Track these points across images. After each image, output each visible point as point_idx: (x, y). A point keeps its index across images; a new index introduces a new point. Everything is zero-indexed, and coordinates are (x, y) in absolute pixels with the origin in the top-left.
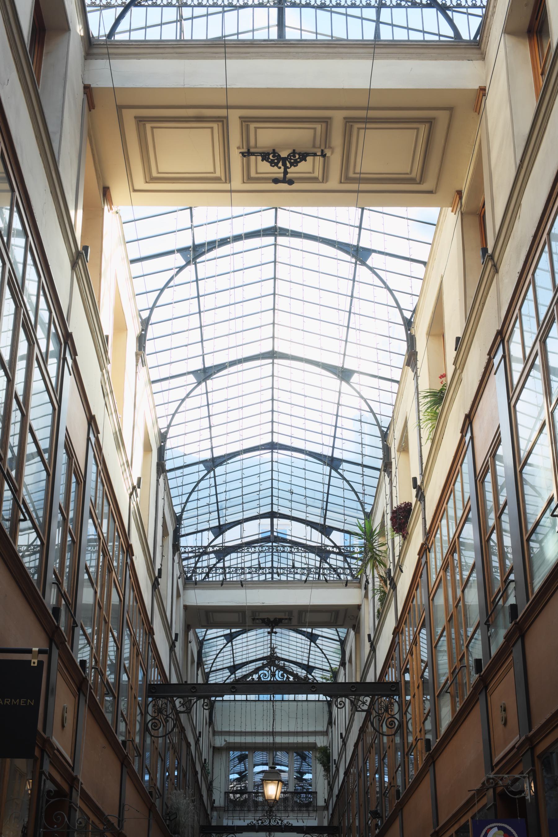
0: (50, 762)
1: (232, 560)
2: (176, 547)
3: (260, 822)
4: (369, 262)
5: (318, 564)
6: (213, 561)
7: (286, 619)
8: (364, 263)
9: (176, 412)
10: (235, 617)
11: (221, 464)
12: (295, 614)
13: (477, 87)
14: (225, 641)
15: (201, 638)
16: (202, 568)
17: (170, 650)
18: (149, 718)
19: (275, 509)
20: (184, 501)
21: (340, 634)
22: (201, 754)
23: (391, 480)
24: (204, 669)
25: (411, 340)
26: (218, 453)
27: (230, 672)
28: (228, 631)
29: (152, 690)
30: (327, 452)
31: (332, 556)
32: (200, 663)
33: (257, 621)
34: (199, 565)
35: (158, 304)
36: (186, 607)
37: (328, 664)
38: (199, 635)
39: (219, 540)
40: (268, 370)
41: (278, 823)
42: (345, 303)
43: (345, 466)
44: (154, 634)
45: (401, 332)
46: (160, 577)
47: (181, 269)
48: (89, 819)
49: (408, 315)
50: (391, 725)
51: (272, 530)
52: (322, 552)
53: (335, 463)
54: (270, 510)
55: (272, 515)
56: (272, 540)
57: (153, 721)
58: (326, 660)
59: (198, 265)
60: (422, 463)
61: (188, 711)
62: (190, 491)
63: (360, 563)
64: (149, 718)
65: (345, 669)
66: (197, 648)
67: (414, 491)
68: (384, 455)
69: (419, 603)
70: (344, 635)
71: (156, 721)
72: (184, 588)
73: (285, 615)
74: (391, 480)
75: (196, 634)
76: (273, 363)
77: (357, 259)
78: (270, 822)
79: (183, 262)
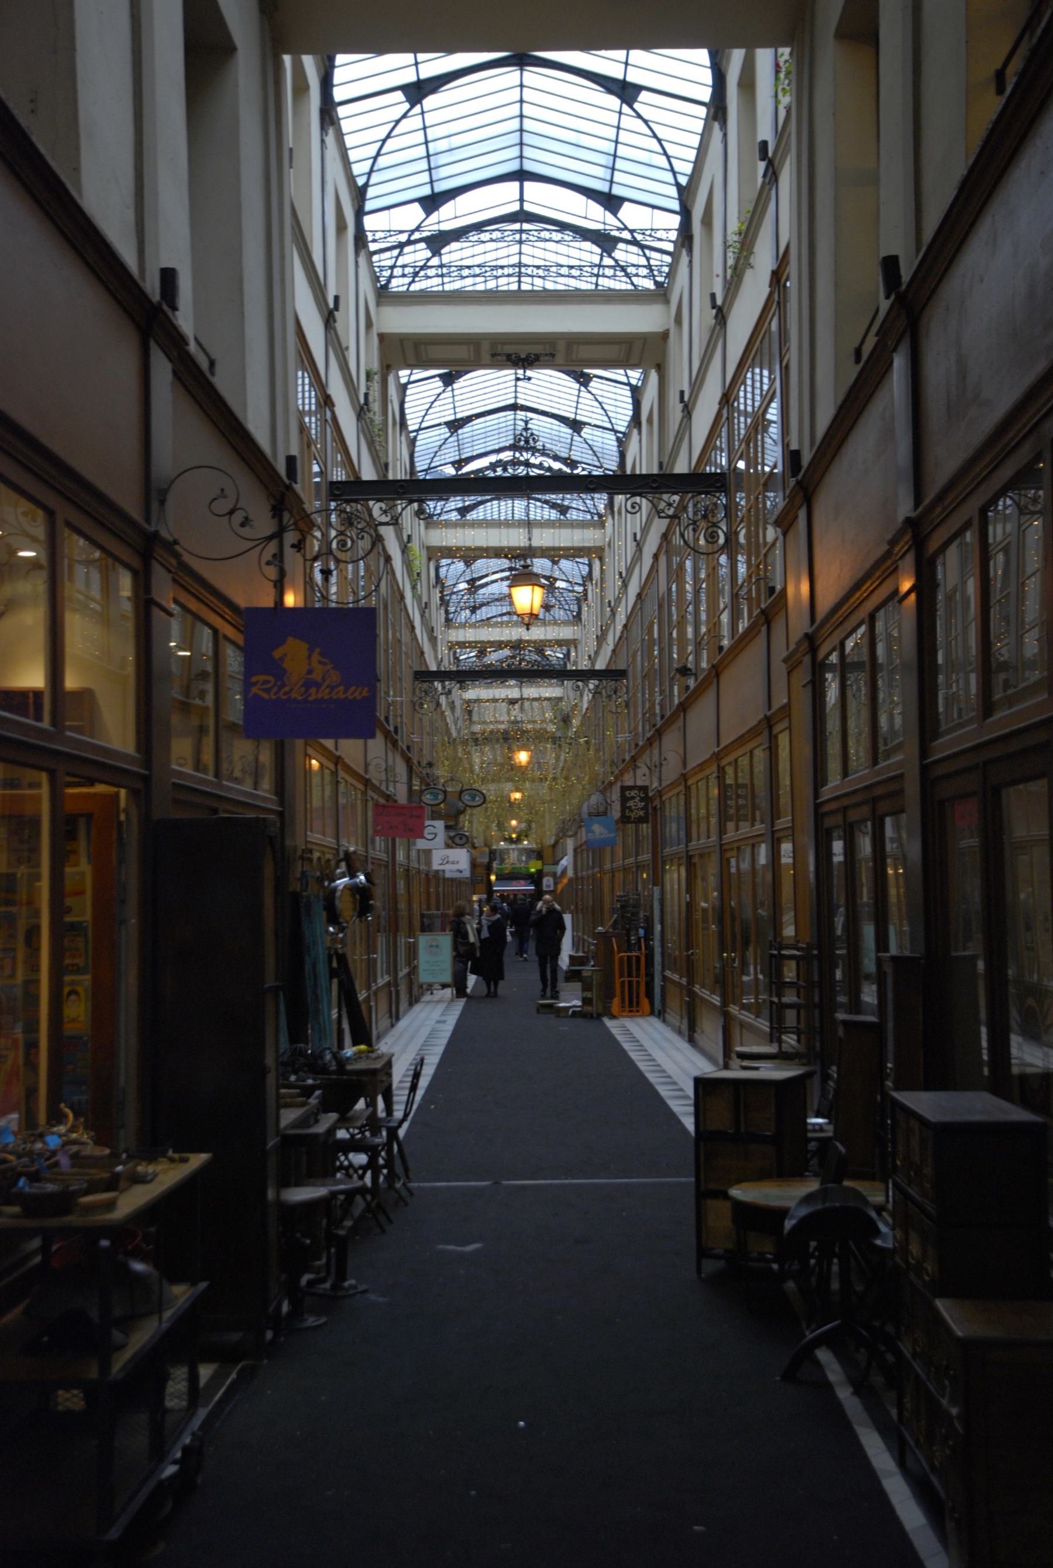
0: (174, 580)
1: (453, 253)
2: (361, 239)
5: (596, 260)
7: (546, 355)
11: (434, 91)
12: (561, 346)
13: (661, 330)
17: (358, 420)
18: (333, 533)
19: (520, 401)
23: (691, 262)
24: (398, 378)
26: (441, 187)
30: (603, 187)
31: (621, 246)
32: (403, 424)
33: (499, 358)
36: (382, 337)
42: (611, 133)
45: (673, 192)
47: (398, 122)
49: (683, 181)
50: (713, 537)
51: (522, 200)
52: (605, 241)
54: (518, 208)
55: (521, 176)
57: (339, 538)
58: (610, 414)
61: (395, 522)
62: (383, 137)
63: (668, 259)
64: (333, 533)
65: (640, 433)
66: (353, 205)
67: (762, 166)
72: (378, 304)
74: (691, 262)
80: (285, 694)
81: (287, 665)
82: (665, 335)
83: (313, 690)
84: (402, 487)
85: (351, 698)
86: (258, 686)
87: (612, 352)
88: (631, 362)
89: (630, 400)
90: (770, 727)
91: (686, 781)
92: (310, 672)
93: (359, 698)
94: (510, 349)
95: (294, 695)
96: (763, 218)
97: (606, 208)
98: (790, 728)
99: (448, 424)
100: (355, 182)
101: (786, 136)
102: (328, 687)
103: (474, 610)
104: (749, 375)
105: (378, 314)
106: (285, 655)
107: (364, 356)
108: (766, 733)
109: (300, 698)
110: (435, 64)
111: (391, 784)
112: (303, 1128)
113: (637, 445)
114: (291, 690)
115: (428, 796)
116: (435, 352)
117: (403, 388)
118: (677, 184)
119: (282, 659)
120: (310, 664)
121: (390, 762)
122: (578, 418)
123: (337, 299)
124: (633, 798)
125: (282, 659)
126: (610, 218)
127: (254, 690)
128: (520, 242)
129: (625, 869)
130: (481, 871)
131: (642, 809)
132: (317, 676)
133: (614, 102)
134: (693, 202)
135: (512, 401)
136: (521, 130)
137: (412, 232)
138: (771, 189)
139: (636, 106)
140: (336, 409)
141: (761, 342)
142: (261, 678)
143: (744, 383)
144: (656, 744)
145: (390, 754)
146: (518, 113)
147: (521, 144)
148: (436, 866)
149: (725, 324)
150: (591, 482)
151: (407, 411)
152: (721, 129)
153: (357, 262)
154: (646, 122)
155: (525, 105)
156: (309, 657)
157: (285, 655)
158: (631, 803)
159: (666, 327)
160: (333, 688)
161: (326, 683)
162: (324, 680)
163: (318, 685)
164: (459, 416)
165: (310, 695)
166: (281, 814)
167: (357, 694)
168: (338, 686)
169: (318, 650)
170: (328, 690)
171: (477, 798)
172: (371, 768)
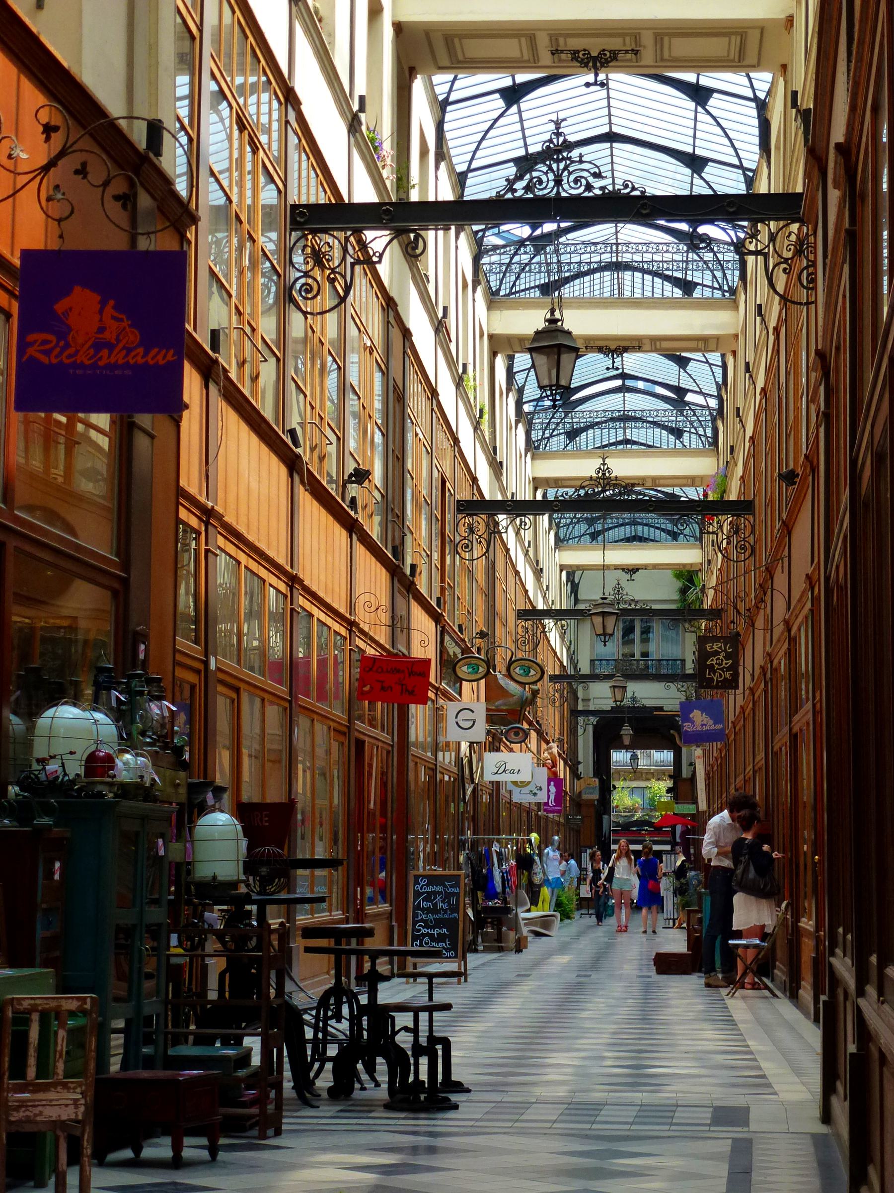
3: (520, 185)
7: (627, 52)
10: (511, 49)
13: (783, 16)
14: (501, 103)
15: (441, 98)
19: (615, 129)
21: (756, 84)
28: (507, 82)
29: (307, 219)
33: (563, 56)
38: (438, 90)
41: (589, 187)
44: (301, 104)
48: (239, 563)
60: (289, 841)
70: (766, 87)
71: (310, 281)
73: (624, 44)
75: (432, 86)
76: (611, 147)
78: (558, 182)
83: (105, 352)
85: (151, 363)
86: (36, 347)
87: (716, 47)
88: (746, 63)
89: (756, 122)
92: (101, 330)
93: (161, 362)
94: (575, 43)
99: (516, 161)
102: (124, 348)
106: (71, 309)
107: (372, 71)
109: (88, 362)
113: (767, 181)
114: (77, 352)
115: (465, 668)
117: (442, 106)
121: (401, 611)
122: (698, 152)
124: (716, 653)
131: (728, 669)
135: (606, 129)
139: (703, 175)
140: (303, 108)
150: (644, 206)
151: (448, 135)
156: (101, 312)
157: (71, 309)
158: (713, 661)
159: (790, 12)
160: (129, 350)
161: (121, 345)
162: (118, 340)
163: (110, 346)
165: (100, 359)
166: (290, 702)
168: (135, 348)
169: (112, 302)
171: (532, 672)
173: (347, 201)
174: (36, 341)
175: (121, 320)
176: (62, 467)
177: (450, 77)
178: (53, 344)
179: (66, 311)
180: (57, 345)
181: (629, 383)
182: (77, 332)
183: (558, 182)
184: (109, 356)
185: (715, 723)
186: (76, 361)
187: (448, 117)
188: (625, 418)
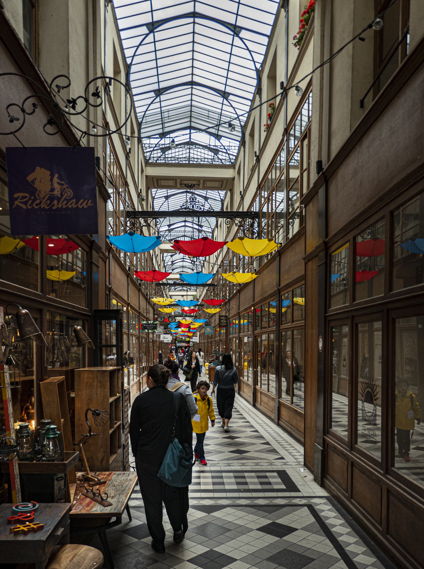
4: (241, 35)
6: (159, 155)
8: (238, 36)
9: (147, 110)
12: (202, 182)
14: (165, 199)
16: (154, 157)
20: (144, 118)
22: (158, 263)
23: (244, 150)
25: (259, 79)
26: (163, 85)
27: (162, 151)
34: (152, 156)
35: (136, 54)
37: (238, 122)
39: (162, 142)
40: (189, 91)
41: (200, 209)
43: (223, 138)
45: (254, 74)
46: (130, 153)
51: (190, 138)
52: (216, 151)
53: (237, 29)
56: (190, 143)
59: (155, 33)
64: (128, 228)
67: (255, 158)
68: (257, 84)
69: (274, 177)
72: (146, 166)
74: (244, 150)
77: (235, 33)
79: (147, 32)
80: (37, 205)
81: (37, 185)
82: (234, 179)
83: (55, 202)
84: (151, 213)
85: (80, 207)
86: (19, 200)
87: (217, 184)
90: (279, 293)
91: (239, 314)
94: (186, 182)
95: (42, 206)
96: (303, 58)
97: (216, 138)
98: (305, 284)
100: (138, 121)
101: (312, 28)
103: (173, 270)
104: (255, 204)
105: (145, 169)
106: (35, 179)
107: (142, 186)
108: (278, 294)
109: (47, 208)
110: (171, 192)
111: (148, 314)
112: (303, 196)
116: (163, 183)
118: (241, 125)
119: (33, 181)
120: (52, 185)
123: (130, 149)
125: (33, 181)
126: (218, 143)
127: (16, 203)
128: (190, 149)
129: (203, 343)
130: (174, 341)
132: (57, 193)
133: (220, 99)
134: (246, 130)
136: (191, 111)
137: (156, 144)
138: (284, 100)
141: (265, 182)
142: (21, 195)
143: (253, 206)
144: (228, 304)
145: (148, 306)
146: (190, 93)
147: (191, 116)
148: (161, 339)
149: (259, 162)
151: (155, 206)
152: (259, 97)
153: (138, 147)
154: (234, 108)
155: (195, 53)
157: (35, 179)
160: (68, 201)
161: (63, 198)
162: (62, 195)
163: (59, 199)
164: (169, 194)
167: (84, 204)
170: (65, 202)
172: (141, 308)
173: (137, 210)
174: (19, 197)
175: (63, 185)
176: (360, 385)
177: (156, 190)
178: (28, 199)
179: (33, 180)
180: (30, 199)
181: (184, 260)
182: (40, 191)
183: (193, 207)
184: (58, 204)
185: (77, 197)
186: (41, 207)
187: (154, 202)
188: (183, 267)
